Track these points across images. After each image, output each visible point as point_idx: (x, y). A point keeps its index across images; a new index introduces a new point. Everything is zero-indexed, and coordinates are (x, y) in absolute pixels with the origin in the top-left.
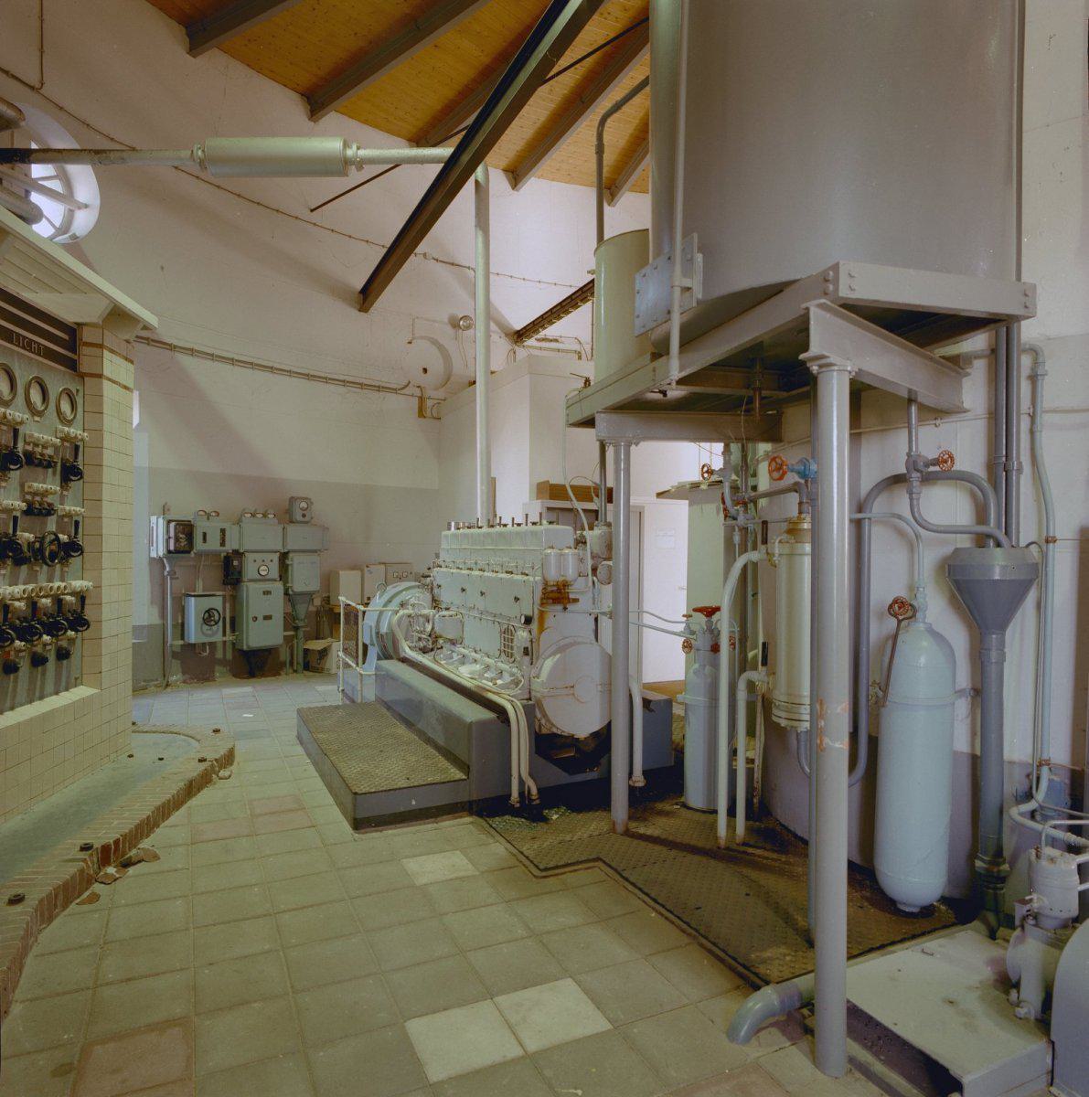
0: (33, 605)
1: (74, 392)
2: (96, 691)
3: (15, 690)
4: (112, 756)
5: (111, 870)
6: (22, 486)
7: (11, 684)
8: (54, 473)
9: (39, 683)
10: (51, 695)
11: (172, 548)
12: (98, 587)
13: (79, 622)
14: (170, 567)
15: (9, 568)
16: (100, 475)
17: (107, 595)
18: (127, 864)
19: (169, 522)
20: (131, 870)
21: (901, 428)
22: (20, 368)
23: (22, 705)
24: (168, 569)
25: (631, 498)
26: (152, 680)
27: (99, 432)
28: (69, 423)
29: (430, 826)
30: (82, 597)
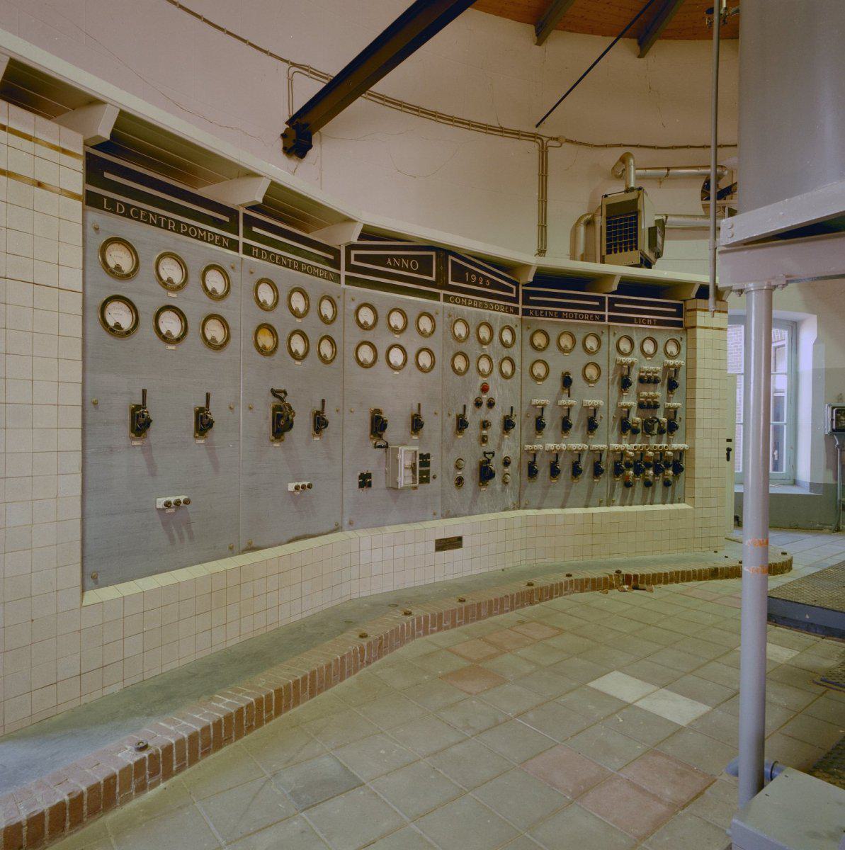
0: (643, 453)
1: (679, 339)
2: (690, 507)
3: (632, 496)
4: (704, 549)
5: (626, 587)
6: (638, 394)
7: (630, 493)
8: (663, 385)
9: (650, 495)
10: (659, 504)
11: (834, 427)
12: (693, 448)
13: (678, 469)
14: (839, 442)
15: (628, 435)
16: (695, 383)
17: (698, 452)
18: (636, 588)
19: (833, 408)
20: (635, 591)
21: (181, 322)
22: (637, 335)
23: (637, 505)
24: (837, 443)
25: (774, 311)
26: (828, 525)
27: (692, 359)
28: (673, 357)
29: (835, 642)
30: (681, 453)
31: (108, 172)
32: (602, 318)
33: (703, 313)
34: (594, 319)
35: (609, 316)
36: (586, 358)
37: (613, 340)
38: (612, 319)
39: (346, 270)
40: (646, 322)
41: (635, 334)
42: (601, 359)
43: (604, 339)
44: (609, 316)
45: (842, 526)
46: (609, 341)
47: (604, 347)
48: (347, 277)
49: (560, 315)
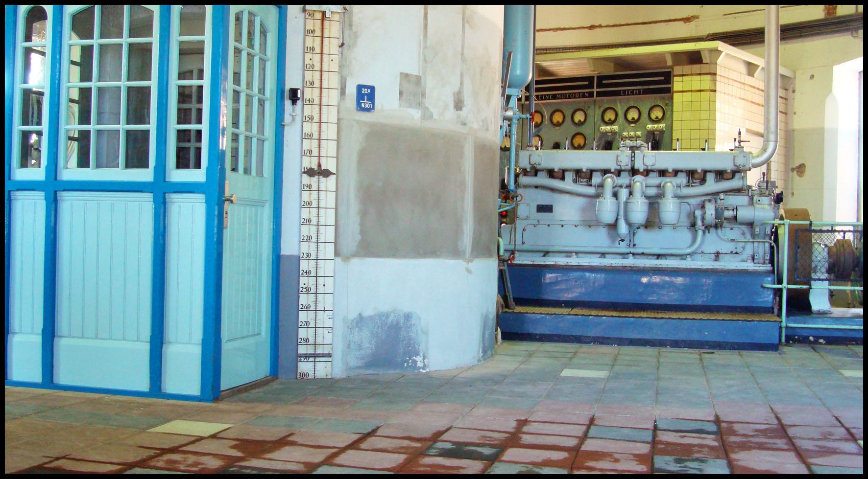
27: (671, 128)
31: (565, 459)
32: (591, 95)
33: (680, 78)
34: (584, 96)
35: (89, 90)
36: (574, 130)
37: (599, 112)
38: (599, 94)
39: (148, 131)
40: (633, 93)
41: (619, 105)
42: (586, 130)
43: (590, 112)
44: (89, 90)
45: (666, 464)
46: (595, 113)
47: (590, 120)
48: (537, 96)
49: (554, 97)
